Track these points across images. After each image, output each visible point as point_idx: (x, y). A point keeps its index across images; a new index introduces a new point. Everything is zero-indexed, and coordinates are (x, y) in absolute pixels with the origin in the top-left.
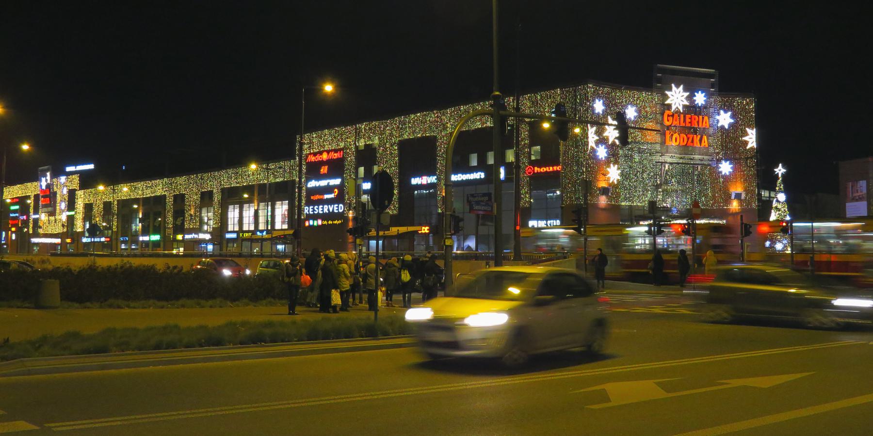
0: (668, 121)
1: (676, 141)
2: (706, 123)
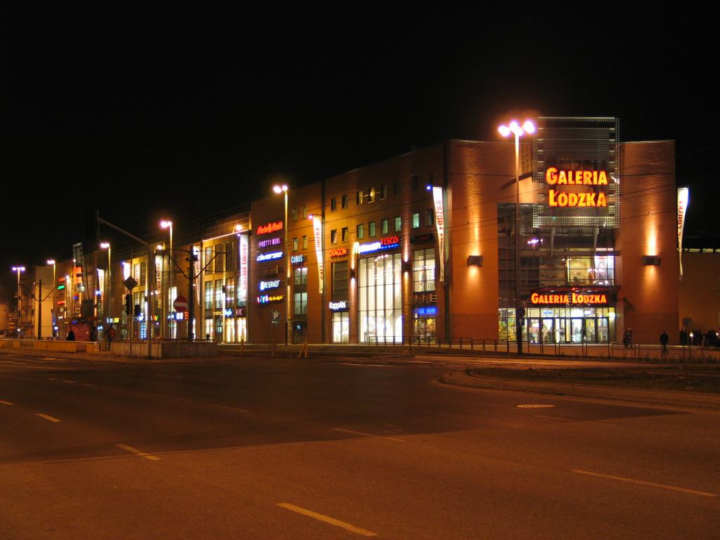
0: (552, 179)
1: (563, 201)
2: (603, 179)
